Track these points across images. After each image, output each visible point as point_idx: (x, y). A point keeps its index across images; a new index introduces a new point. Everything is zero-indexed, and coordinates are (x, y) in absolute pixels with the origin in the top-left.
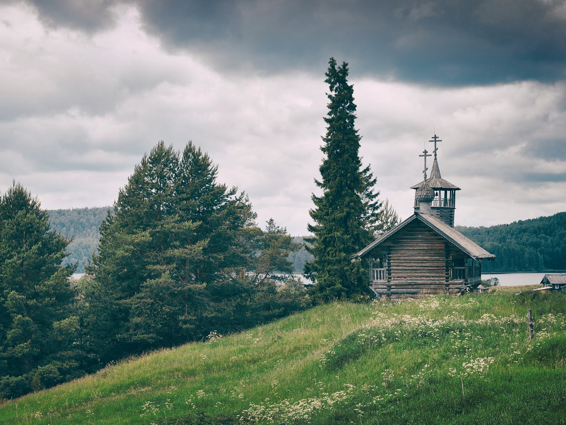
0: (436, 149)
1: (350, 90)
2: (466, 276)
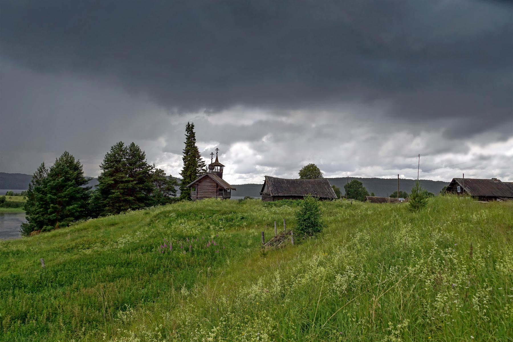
1: (194, 134)
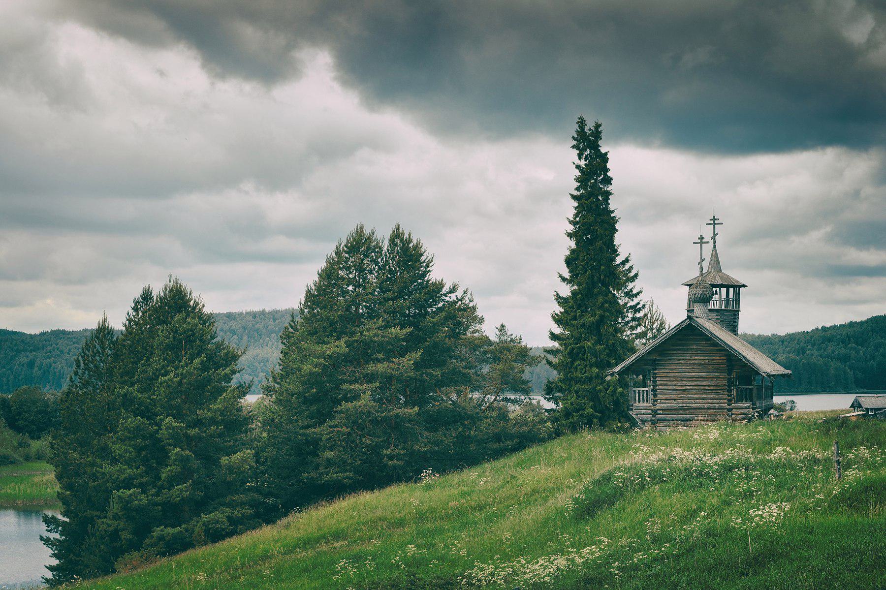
0: (715, 235)
2: (754, 399)
